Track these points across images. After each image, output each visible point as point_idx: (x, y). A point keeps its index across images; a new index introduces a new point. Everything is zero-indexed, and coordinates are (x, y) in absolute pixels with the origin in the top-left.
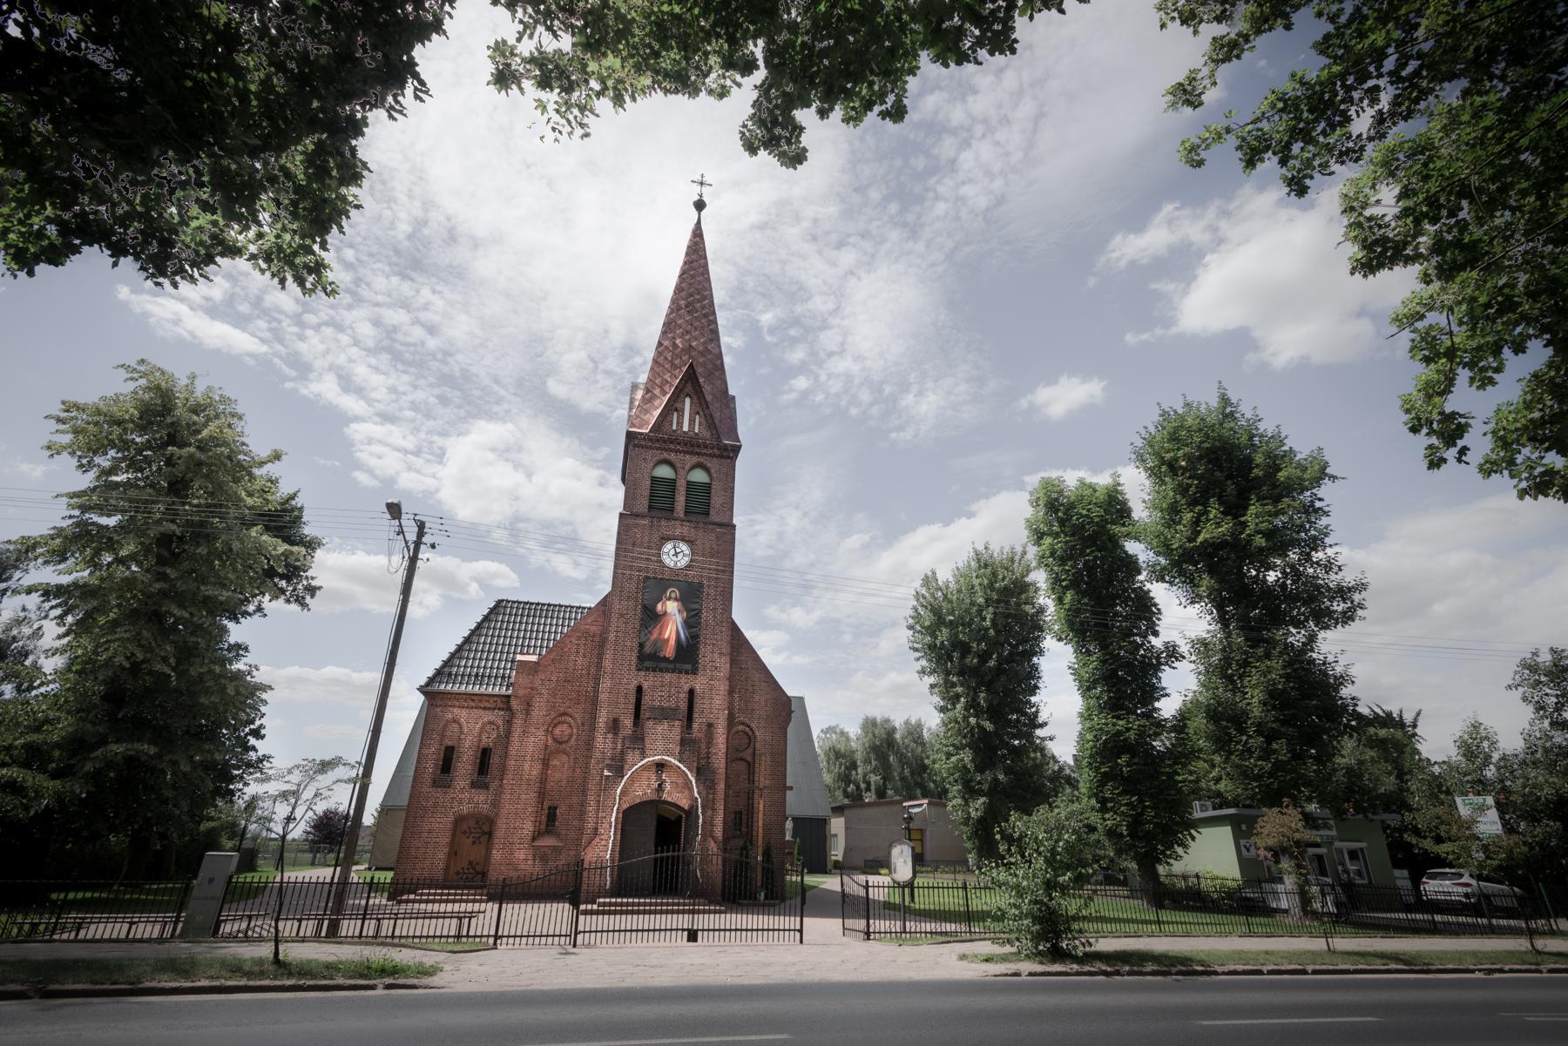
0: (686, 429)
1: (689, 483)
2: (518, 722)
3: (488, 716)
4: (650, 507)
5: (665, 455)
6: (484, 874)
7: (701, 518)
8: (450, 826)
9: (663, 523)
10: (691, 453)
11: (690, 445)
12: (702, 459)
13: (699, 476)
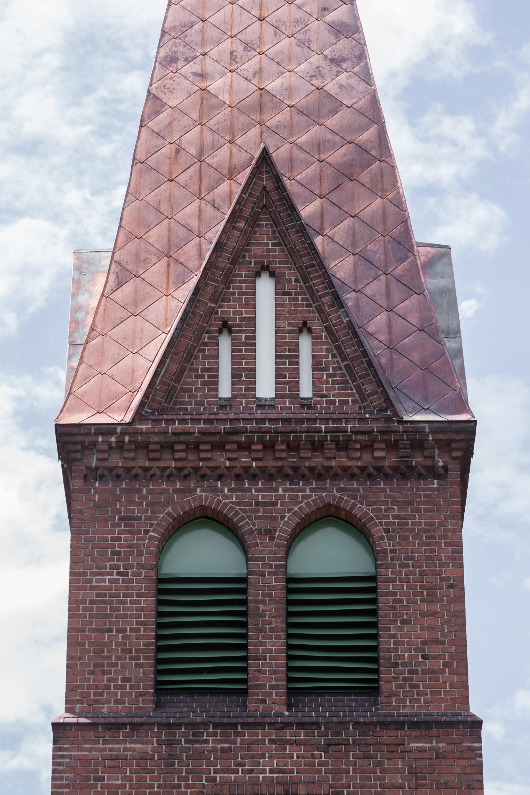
0: (266, 387)
1: (294, 584)
4: (162, 690)
5: (200, 495)
7: (349, 709)
9: (211, 742)
10: (295, 475)
11: (282, 446)
12: (332, 493)
13: (328, 555)
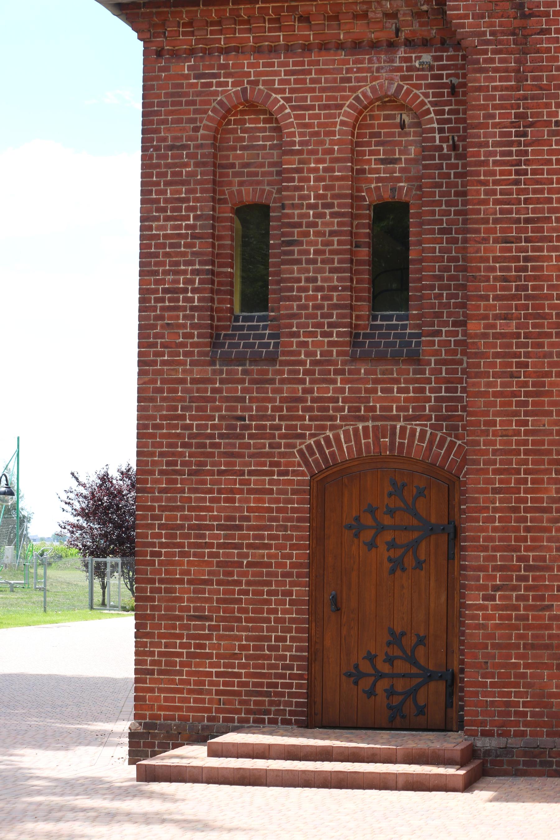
2: (490, 83)
6: (452, 682)
8: (299, 505)
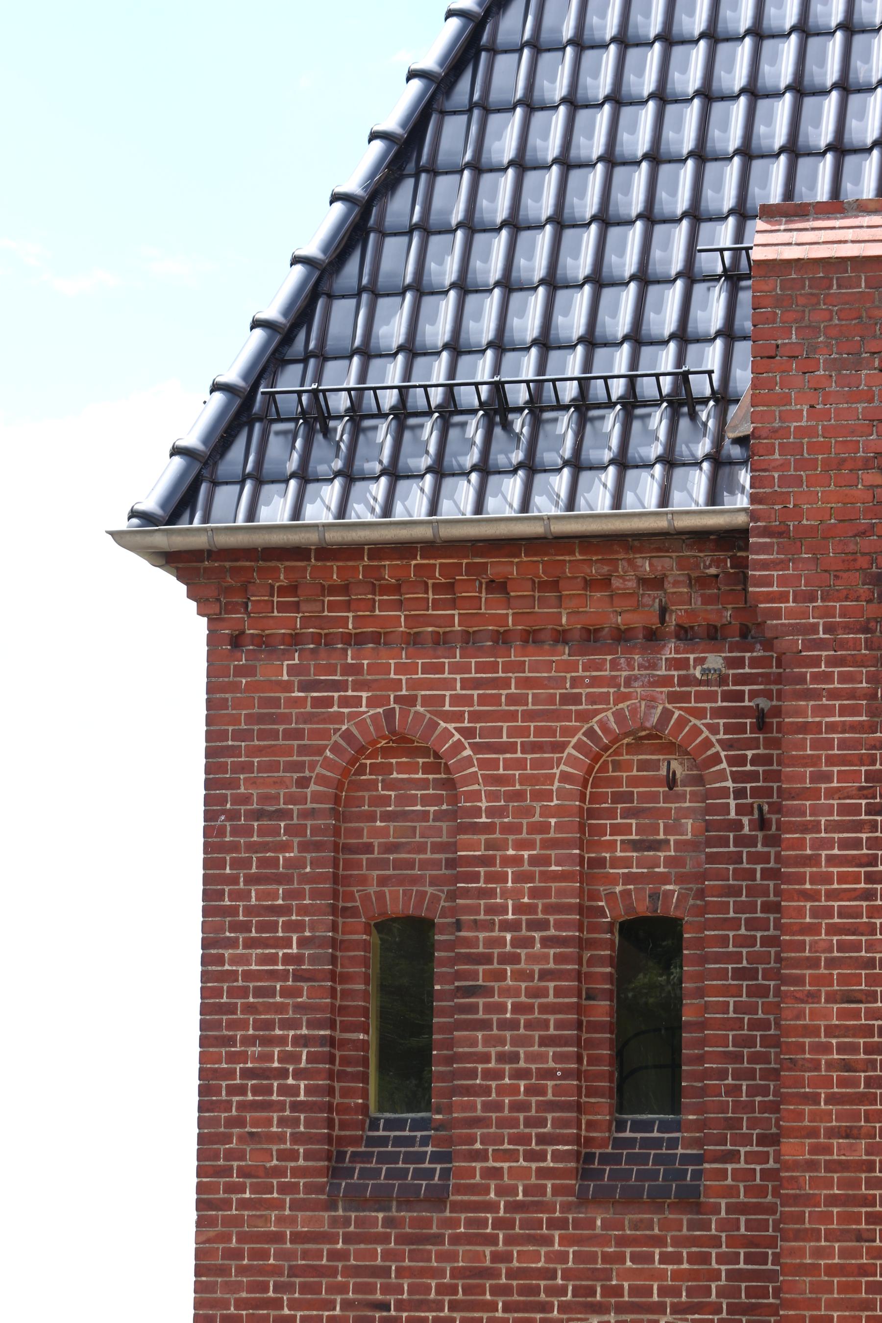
3: (633, 691)
